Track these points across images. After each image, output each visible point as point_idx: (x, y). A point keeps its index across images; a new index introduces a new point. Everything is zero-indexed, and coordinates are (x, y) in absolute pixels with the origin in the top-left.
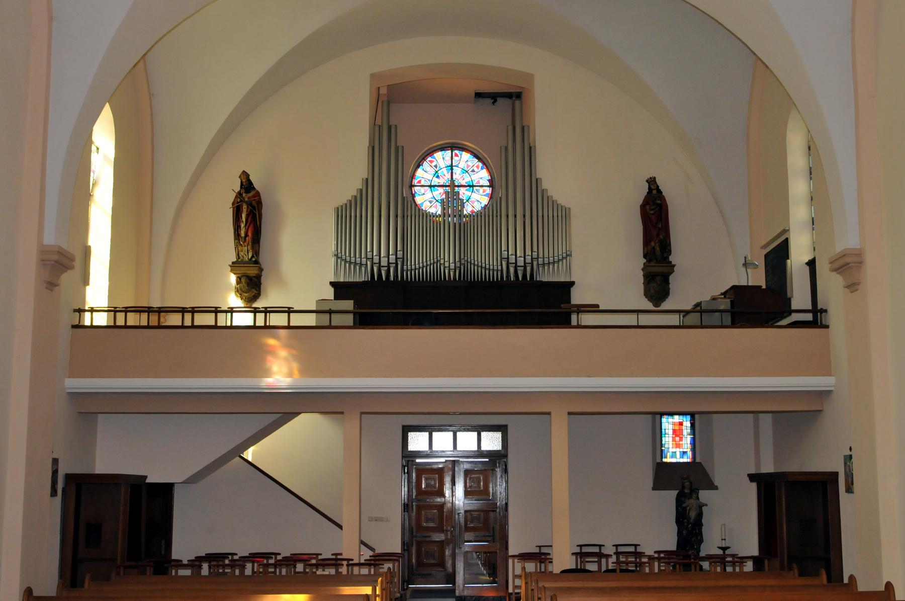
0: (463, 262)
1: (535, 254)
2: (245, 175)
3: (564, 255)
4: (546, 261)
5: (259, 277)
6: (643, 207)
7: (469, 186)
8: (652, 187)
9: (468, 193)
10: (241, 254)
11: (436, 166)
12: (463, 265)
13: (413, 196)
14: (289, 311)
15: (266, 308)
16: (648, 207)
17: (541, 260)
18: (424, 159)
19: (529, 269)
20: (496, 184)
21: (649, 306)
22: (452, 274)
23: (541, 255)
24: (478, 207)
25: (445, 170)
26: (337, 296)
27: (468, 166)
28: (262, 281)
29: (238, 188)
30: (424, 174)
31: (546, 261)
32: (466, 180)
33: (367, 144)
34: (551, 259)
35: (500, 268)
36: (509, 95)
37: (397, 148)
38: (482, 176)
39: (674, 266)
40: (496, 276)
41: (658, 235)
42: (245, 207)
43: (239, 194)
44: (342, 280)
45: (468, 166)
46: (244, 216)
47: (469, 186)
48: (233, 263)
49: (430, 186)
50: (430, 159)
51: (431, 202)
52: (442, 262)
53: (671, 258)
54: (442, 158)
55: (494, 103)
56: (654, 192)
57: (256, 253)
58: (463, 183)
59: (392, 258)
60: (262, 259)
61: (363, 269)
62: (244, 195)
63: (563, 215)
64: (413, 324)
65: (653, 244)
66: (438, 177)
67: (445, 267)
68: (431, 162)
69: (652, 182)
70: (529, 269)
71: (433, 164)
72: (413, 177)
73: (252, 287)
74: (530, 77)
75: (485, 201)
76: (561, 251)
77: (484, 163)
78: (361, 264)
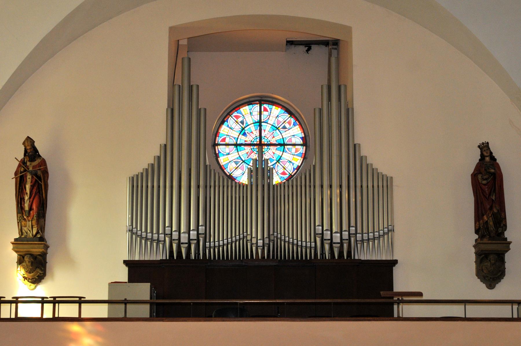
0: (272, 238)
1: (353, 230)
2: (29, 142)
3: (386, 230)
4: (365, 236)
5: (44, 255)
6: (474, 176)
7: (280, 145)
8: (485, 154)
9: (279, 153)
10: (25, 229)
11: (242, 122)
12: (272, 241)
13: (217, 156)
14: (80, 301)
15: (55, 298)
16: (480, 177)
17: (359, 236)
18: (229, 114)
19: (345, 246)
20: (311, 143)
21: (481, 291)
22: (260, 251)
23: (359, 231)
24: (290, 169)
25: (252, 128)
26: (133, 278)
27: (279, 122)
28: (48, 260)
29: (21, 156)
30: (229, 131)
31: (365, 236)
32: (277, 138)
33: (166, 105)
34: (371, 235)
35: (313, 245)
36: (325, 43)
37: (199, 111)
38: (295, 133)
39: (510, 243)
40: (310, 255)
41: (491, 208)
42: (29, 177)
43: (23, 163)
44: (137, 258)
45: (279, 122)
46: (28, 187)
47: (280, 145)
48: (16, 240)
49: (236, 145)
50: (235, 114)
51: (236, 163)
52: (249, 238)
53: (507, 234)
54: (249, 113)
55: (308, 51)
56: (487, 159)
57: (42, 228)
58: (273, 141)
59: (193, 234)
60: (47, 236)
61: (161, 245)
62: (28, 163)
63: (386, 184)
64: (216, 316)
65: (485, 218)
66: (244, 134)
67: (252, 244)
68: (237, 117)
69: (484, 148)
70: (345, 246)
71: (240, 120)
72: (217, 134)
73: (37, 266)
74: (348, 30)
75: (298, 161)
76: (382, 225)
77: (296, 119)
78: (158, 241)
